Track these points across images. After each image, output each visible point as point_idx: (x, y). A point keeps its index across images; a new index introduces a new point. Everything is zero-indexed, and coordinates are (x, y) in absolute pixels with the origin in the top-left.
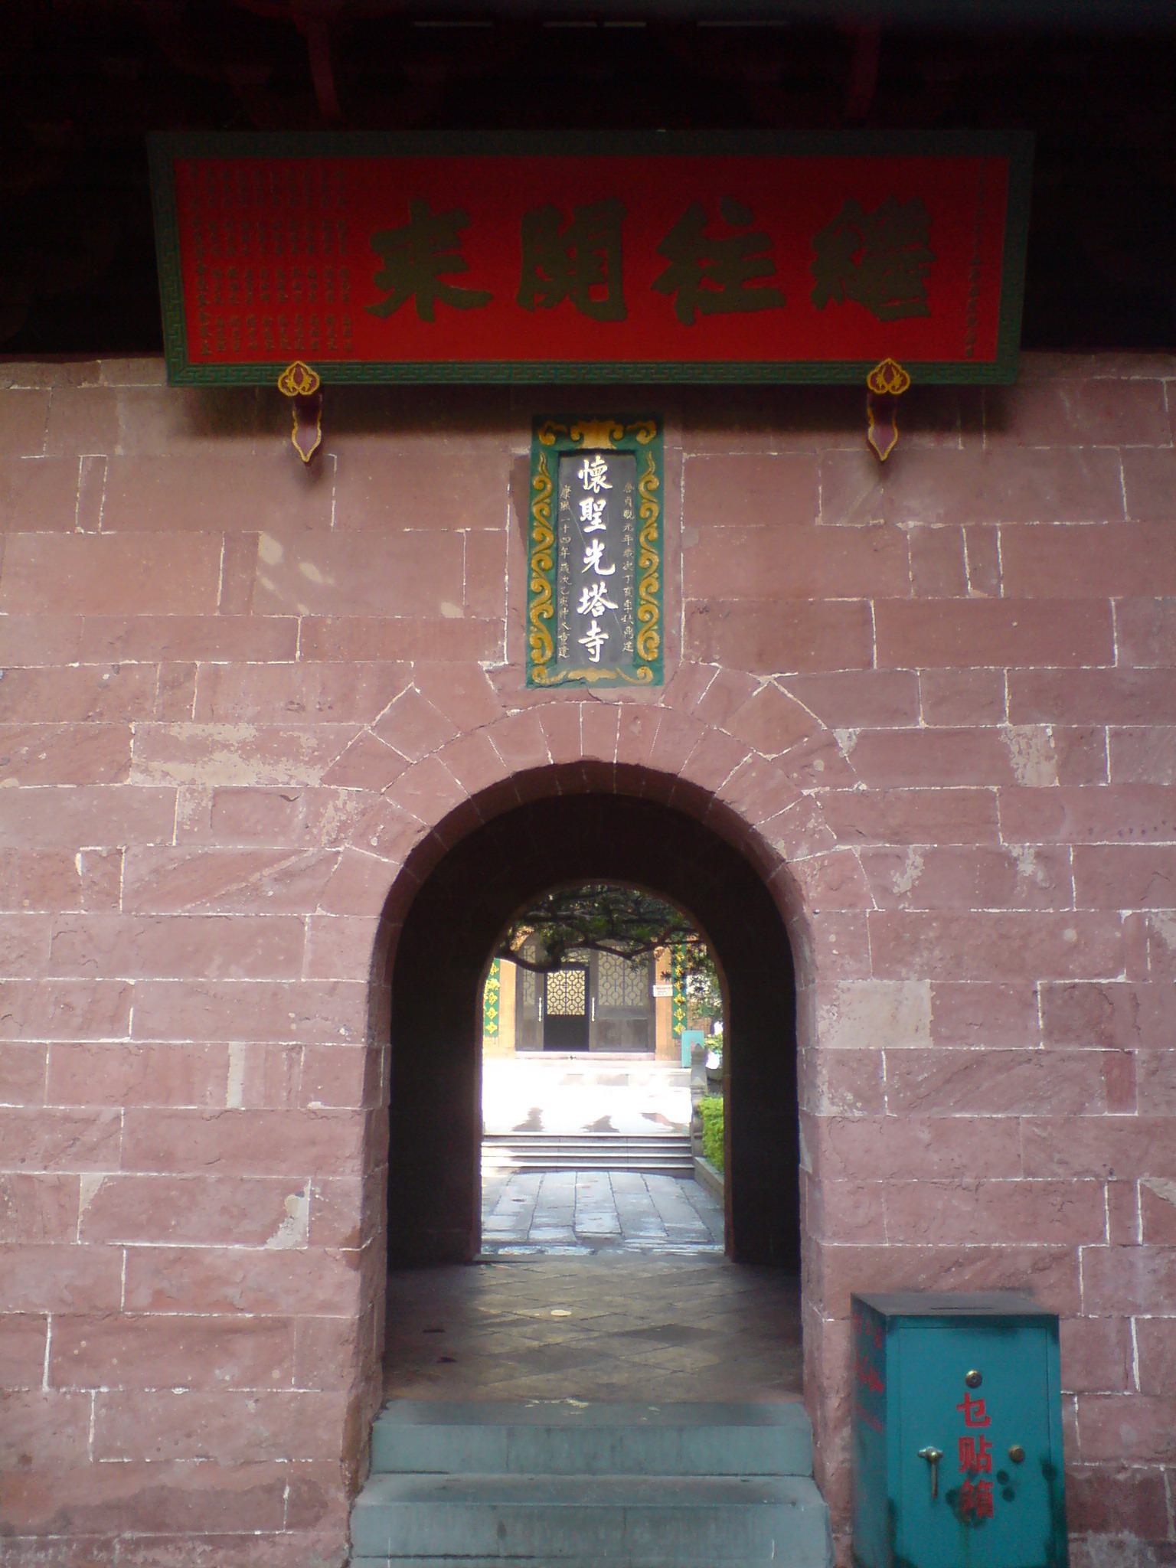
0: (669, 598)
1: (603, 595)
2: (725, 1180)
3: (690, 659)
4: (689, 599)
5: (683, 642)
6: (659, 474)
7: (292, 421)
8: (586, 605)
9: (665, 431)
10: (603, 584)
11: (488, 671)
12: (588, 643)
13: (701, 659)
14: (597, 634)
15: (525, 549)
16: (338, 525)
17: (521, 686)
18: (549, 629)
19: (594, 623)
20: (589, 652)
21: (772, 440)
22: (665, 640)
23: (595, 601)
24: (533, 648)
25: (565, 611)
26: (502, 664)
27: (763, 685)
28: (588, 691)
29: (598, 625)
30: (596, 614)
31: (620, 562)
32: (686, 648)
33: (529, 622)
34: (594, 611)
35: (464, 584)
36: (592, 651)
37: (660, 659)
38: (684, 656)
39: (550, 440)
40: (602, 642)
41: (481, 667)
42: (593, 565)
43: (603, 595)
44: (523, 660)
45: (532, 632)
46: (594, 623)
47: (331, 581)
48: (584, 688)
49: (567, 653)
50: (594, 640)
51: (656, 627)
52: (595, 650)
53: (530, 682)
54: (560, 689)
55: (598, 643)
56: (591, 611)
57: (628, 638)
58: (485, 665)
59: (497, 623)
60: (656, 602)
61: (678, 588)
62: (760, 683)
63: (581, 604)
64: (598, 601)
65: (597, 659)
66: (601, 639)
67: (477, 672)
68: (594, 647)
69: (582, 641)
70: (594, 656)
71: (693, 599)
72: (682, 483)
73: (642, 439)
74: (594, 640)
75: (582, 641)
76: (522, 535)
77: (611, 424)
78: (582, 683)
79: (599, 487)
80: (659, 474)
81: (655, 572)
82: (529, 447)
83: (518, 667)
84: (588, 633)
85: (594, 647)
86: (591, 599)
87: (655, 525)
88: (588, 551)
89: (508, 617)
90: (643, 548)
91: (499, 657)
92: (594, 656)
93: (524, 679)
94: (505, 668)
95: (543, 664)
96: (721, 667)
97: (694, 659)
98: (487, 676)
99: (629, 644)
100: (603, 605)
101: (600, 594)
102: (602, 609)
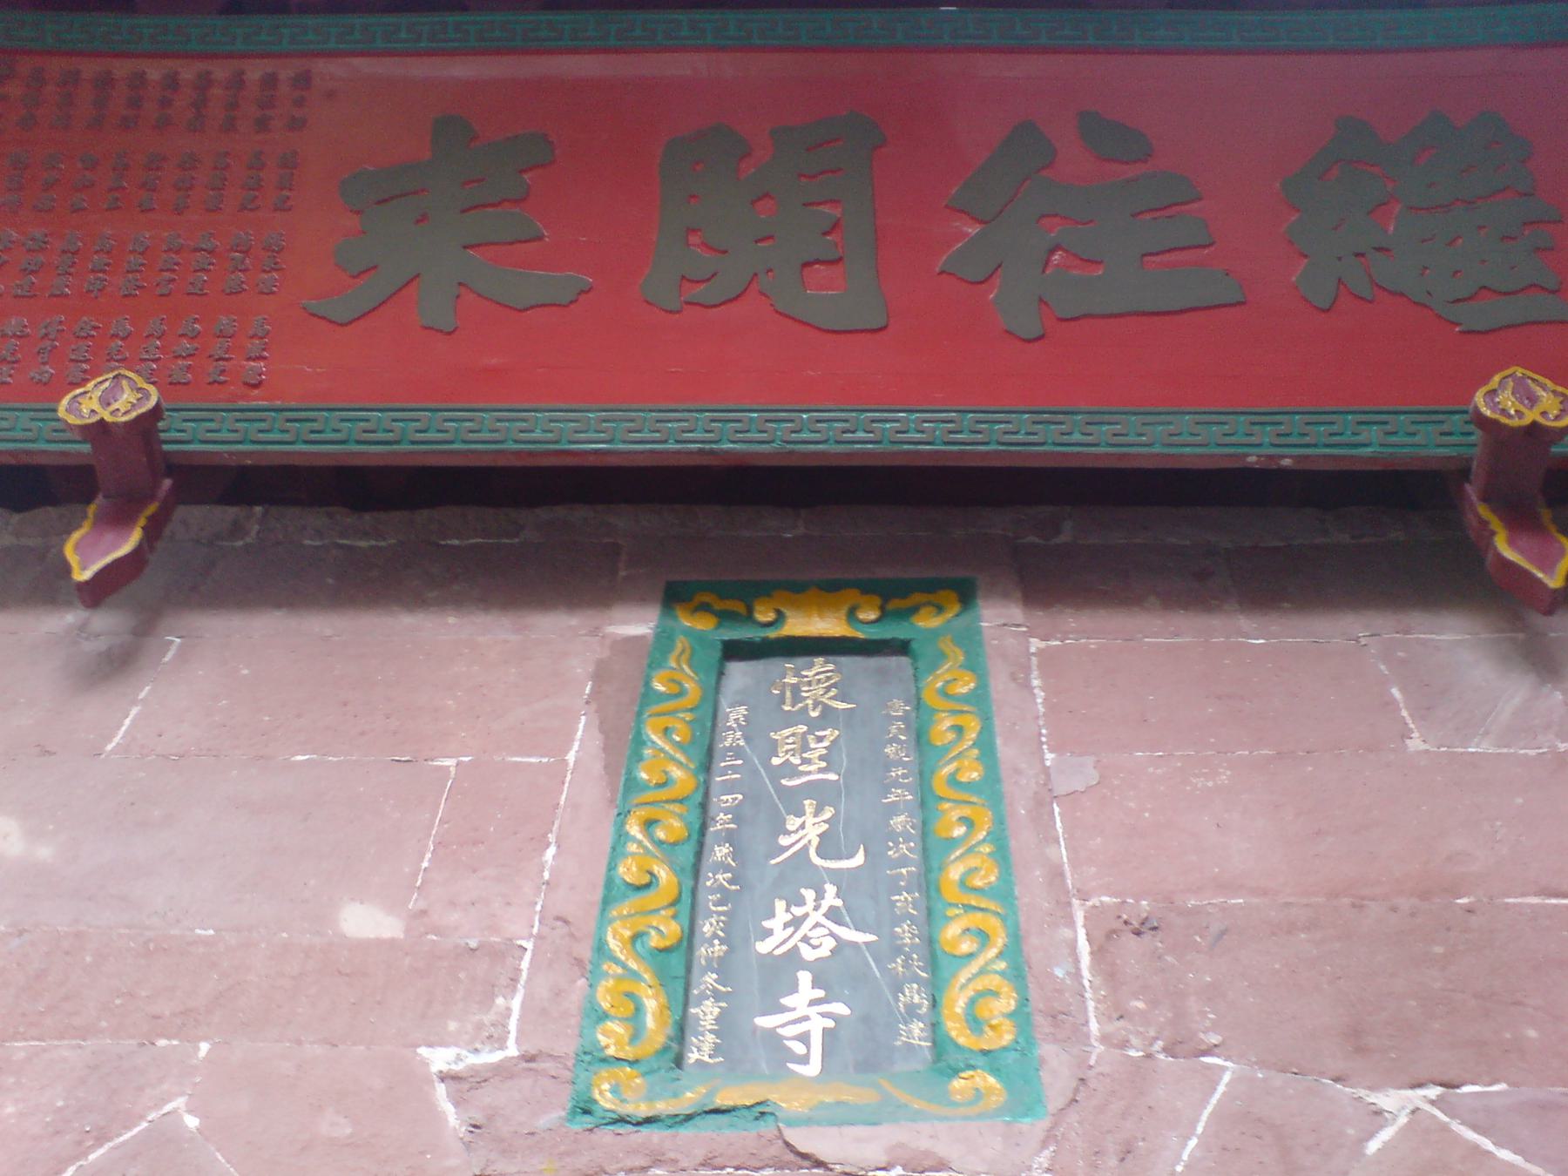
0: (1032, 892)
1: (832, 914)
2: (183, 1121)
3: (1124, 1044)
4: (1094, 901)
5: (1091, 1005)
6: (974, 665)
7: (85, 517)
8: (780, 934)
9: (980, 602)
10: (831, 890)
11: (444, 1077)
12: (783, 1026)
13: (1160, 1043)
14: (814, 1002)
15: (614, 791)
16: (123, 749)
17: (550, 1118)
18: (663, 978)
19: (805, 978)
20: (789, 1049)
21: (1244, 622)
22: (1033, 993)
23: (805, 929)
24: (605, 1016)
25: (718, 949)
26: (496, 1057)
27: (1395, 1117)
28: (781, 1135)
29: (816, 984)
30: (808, 954)
31: (875, 839)
32: (1103, 1017)
33: (601, 949)
34: (804, 948)
35: (425, 864)
36: (799, 1049)
37: (1024, 1046)
38: (1105, 1039)
39: (703, 624)
40: (830, 1024)
41: (425, 1064)
42: (805, 848)
43: (832, 914)
44: (567, 1047)
45: (606, 975)
46: (805, 978)
47: (45, 852)
48: (767, 1128)
49: (716, 1051)
50: (806, 1018)
51: (1002, 965)
52: (807, 1044)
53: (585, 1109)
54: (686, 1132)
55: (817, 1027)
56: (796, 947)
57: (912, 1012)
58: (440, 1059)
59: (503, 953)
60: (992, 907)
61: (1056, 874)
62: (1379, 1113)
63: (769, 933)
64: (817, 925)
65: (813, 1068)
66: (824, 1015)
67: (415, 1080)
68: (804, 1038)
69: (765, 1022)
70: (805, 1060)
71: (1106, 899)
72: (1036, 683)
73: (927, 622)
74: (806, 1018)
75: (765, 1022)
76: (610, 769)
77: (852, 595)
78: (763, 1114)
79: (820, 708)
80: (974, 665)
81: (971, 747)
82: (652, 625)
83: (547, 1065)
84: (785, 1001)
85: (804, 1038)
86: (796, 923)
87: (986, 849)
88: (792, 823)
89: (540, 937)
90: (941, 798)
91: (490, 1037)
92: (805, 1060)
93: (565, 1098)
94: (502, 1071)
95: (633, 1063)
96: (1229, 1064)
97: (1134, 1041)
98: (441, 1089)
99: (917, 1027)
100: (832, 934)
101: (824, 909)
102: (830, 943)
